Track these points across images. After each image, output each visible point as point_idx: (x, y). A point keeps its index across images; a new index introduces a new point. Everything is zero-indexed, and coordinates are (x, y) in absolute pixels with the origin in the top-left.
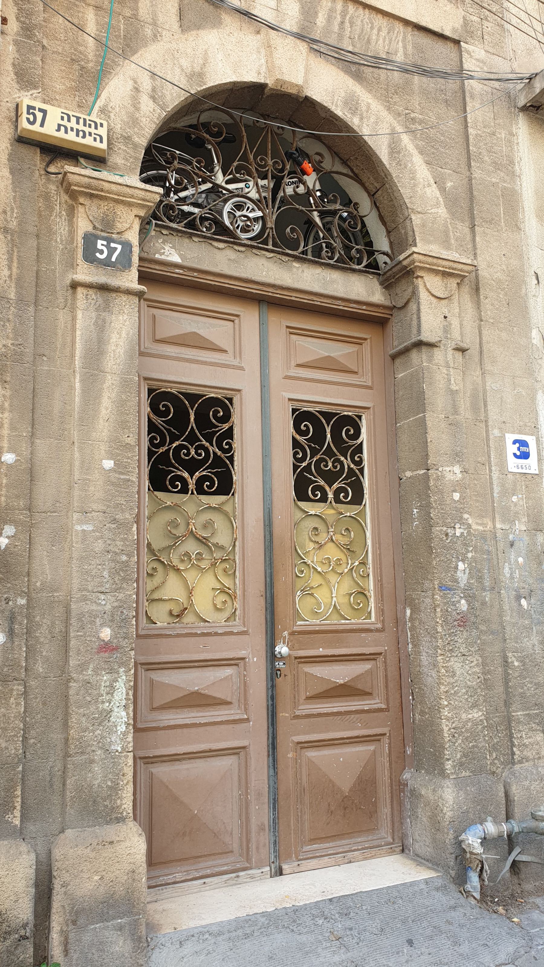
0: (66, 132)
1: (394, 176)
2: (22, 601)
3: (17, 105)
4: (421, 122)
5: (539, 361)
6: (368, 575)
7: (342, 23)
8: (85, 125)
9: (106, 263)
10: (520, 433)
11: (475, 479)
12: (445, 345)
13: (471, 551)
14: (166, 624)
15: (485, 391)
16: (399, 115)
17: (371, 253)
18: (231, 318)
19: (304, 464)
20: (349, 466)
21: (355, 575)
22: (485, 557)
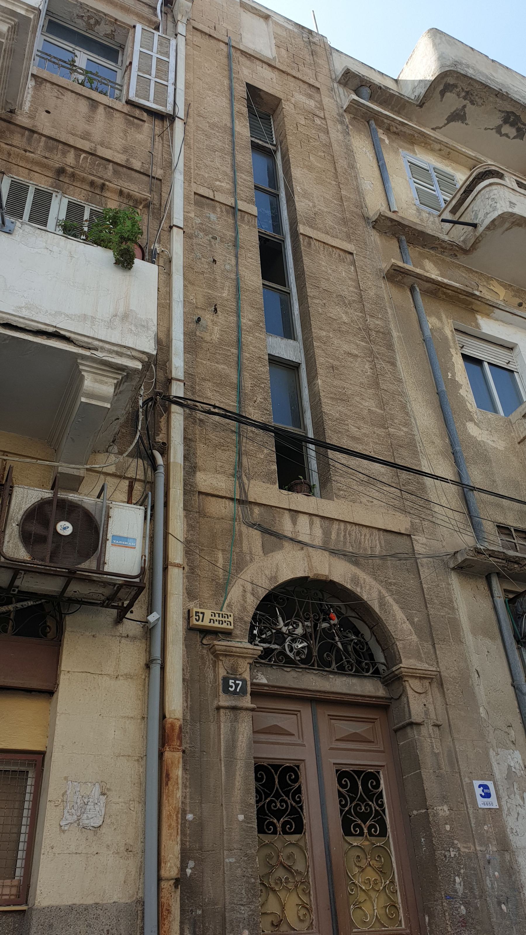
0: (214, 623)
1: (383, 619)
2: (199, 912)
3: (189, 611)
4: (395, 584)
5: (487, 728)
6: (397, 891)
7: (345, 535)
8: (222, 617)
9: (235, 693)
10: (482, 779)
11: (458, 814)
12: (427, 723)
13: (463, 868)
14: (270, 932)
15: (456, 751)
16: (382, 582)
17: (374, 664)
18: (295, 713)
19: (346, 809)
20: (375, 808)
21: (387, 891)
22: (473, 872)
